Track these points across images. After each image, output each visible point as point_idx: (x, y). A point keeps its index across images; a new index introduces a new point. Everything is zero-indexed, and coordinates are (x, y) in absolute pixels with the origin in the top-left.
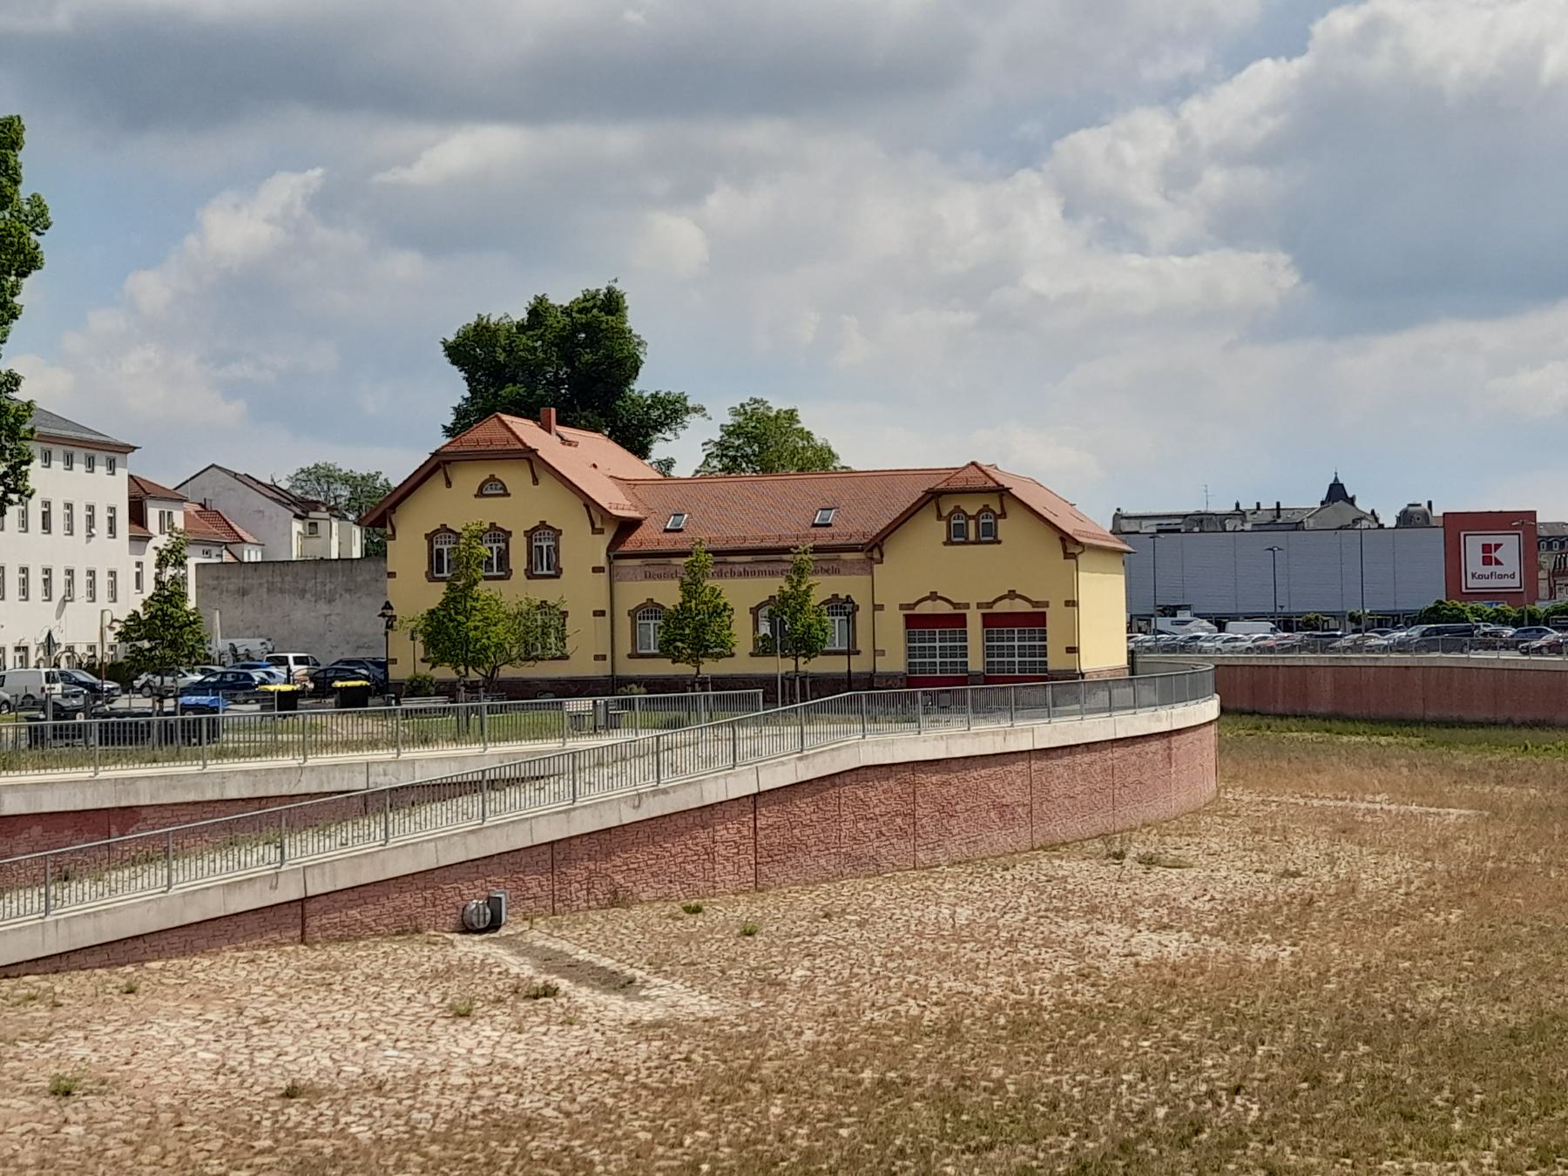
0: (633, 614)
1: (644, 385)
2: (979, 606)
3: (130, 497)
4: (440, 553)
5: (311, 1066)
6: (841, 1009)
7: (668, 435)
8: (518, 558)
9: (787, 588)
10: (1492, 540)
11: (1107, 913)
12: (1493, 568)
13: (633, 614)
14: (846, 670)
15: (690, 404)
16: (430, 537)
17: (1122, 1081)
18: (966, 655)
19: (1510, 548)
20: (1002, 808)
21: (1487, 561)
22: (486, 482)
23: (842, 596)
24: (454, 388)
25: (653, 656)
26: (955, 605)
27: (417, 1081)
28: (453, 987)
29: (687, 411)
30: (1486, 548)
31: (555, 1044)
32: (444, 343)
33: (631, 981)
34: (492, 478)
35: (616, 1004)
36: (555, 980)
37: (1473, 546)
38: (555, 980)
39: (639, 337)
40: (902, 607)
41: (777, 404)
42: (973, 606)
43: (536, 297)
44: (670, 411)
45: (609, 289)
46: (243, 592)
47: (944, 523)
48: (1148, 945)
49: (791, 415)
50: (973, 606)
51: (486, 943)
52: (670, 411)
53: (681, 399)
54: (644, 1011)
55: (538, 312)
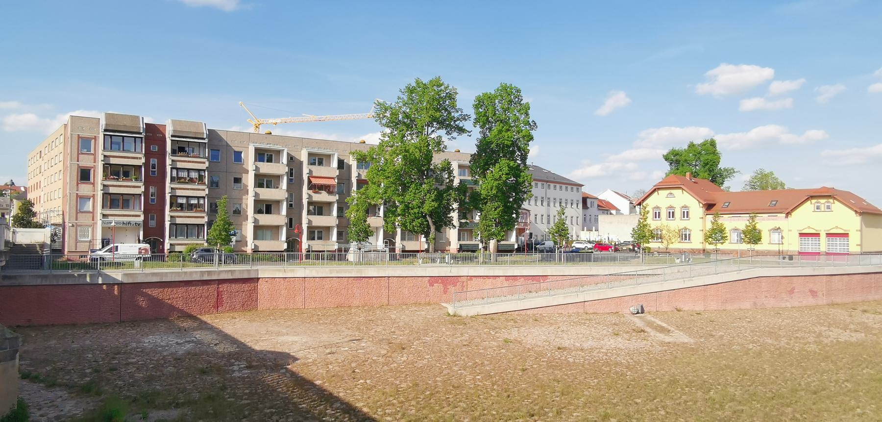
1: (722, 165)
2: (825, 231)
3: (259, 187)
5: (566, 344)
7: (729, 179)
8: (678, 214)
9: (748, 224)
14: (778, 249)
17: (806, 374)
18: (820, 246)
22: (669, 193)
23: (778, 227)
25: (735, 243)
26: (845, 230)
27: (592, 349)
28: (617, 328)
29: (734, 172)
31: (636, 343)
32: (663, 155)
33: (670, 331)
35: (661, 337)
36: (648, 329)
38: (648, 329)
40: (798, 231)
41: (767, 171)
42: (823, 231)
43: (690, 142)
44: (730, 172)
47: (813, 205)
48: (844, 336)
49: (772, 173)
50: (823, 231)
51: (74, 260)
52: (730, 172)
54: (668, 339)
55: (692, 145)
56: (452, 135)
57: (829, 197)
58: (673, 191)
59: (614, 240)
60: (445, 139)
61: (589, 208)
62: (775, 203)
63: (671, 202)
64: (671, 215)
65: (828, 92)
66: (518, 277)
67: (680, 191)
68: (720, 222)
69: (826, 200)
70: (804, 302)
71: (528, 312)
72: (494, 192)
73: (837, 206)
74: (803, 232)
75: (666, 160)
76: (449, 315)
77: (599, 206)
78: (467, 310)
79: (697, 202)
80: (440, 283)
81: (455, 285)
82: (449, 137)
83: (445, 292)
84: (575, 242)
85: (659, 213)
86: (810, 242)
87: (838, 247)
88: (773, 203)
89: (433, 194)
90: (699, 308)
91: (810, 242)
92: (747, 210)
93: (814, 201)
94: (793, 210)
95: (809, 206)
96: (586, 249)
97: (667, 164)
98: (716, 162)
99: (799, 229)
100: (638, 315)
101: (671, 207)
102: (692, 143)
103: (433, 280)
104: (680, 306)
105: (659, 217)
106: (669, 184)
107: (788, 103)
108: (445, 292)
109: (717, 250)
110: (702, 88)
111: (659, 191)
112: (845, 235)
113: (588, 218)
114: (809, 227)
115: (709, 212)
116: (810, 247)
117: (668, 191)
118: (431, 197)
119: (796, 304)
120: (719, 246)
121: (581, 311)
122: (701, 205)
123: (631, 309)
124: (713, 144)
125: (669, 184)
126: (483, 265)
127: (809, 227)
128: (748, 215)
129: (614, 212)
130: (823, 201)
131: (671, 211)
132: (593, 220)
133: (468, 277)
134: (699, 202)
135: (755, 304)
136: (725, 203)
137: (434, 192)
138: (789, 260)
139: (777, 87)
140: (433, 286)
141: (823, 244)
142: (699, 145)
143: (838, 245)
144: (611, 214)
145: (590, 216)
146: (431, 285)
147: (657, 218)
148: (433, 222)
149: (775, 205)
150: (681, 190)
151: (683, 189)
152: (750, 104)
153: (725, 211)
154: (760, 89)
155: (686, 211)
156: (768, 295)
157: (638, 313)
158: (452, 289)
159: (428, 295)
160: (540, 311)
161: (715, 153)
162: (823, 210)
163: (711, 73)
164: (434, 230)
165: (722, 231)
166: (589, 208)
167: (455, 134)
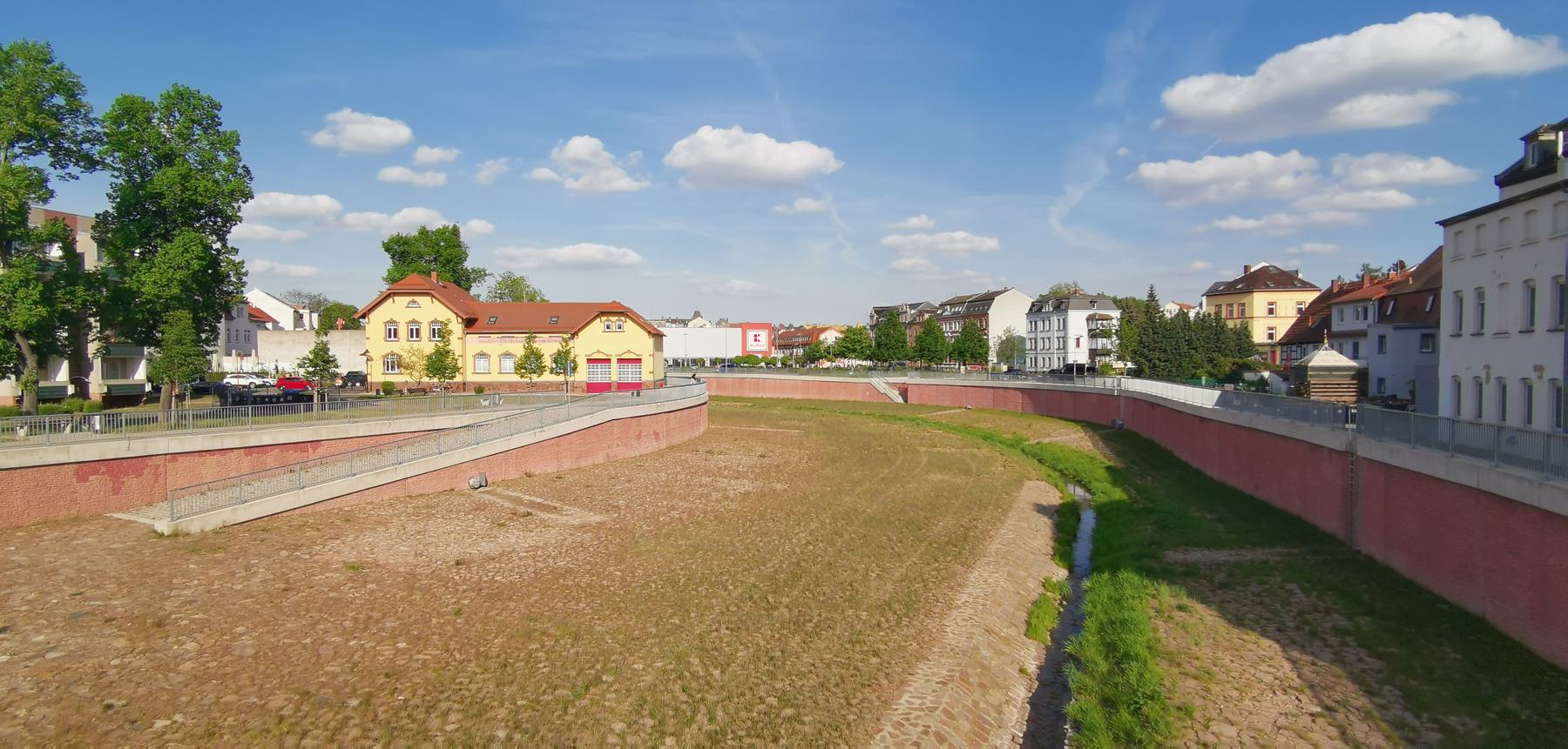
0: (474, 356)
1: (469, 264)
4: (434, 330)
6: (709, 509)
9: (561, 349)
10: (757, 333)
11: (28, 577)
12: (758, 343)
13: (474, 356)
15: (487, 272)
16: (386, 323)
19: (764, 335)
20: (656, 434)
21: (755, 340)
24: (386, 262)
26: (638, 355)
29: (486, 275)
30: (755, 336)
32: (383, 243)
34: (414, 302)
37: (751, 334)
39: (872, 317)
44: (480, 275)
45: (455, 226)
46: (281, 343)
52: (480, 275)
53: (484, 271)
56: (67, 171)
57: (622, 314)
58: (416, 298)
59: (287, 370)
60: (53, 175)
61: (234, 318)
62: (494, 319)
63: (414, 314)
64: (415, 333)
65: (489, 171)
66: (269, 448)
67: (429, 298)
68: (535, 345)
69: (617, 318)
70: (650, 448)
71: (318, 508)
72: (176, 291)
73: (629, 326)
74: (592, 357)
75: (387, 250)
76: (161, 535)
77: (250, 315)
78: (205, 518)
79: (455, 316)
80: (103, 473)
81: (138, 473)
82: (60, 172)
83: (116, 491)
84: (228, 376)
85: (395, 329)
86: (599, 370)
87: (599, 376)
88: (492, 320)
89: (34, 289)
90: (552, 469)
91: (599, 370)
92: (522, 328)
93: (604, 318)
94: (580, 330)
95: (598, 325)
96: (252, 386)
97: (388, 256)
98: (462, 257)
99: (587, 353)
100: (481, 489)
101: (414, 322)
102: (424, 227)
103: (86, 468)
104: (531, 470)
105: (417, 336)
106: (403, 287)
107: (441, 178)
108: (116, 491)
109: (534, 385)
110: (322, 138)
111: (395, 298)
112: (639, 361)
113: (233, 334)
114: (599, 352)
115: (470, 330)
116: (630, 376)
117: (410, 298)
118: (32, 295)
119: (644, 451)
120: (535, 378)
121: (401, 494)
122: (460, 320)
123: (471, 481)
124: (455, 232)
125: (403, 287)
126: (179, 431)
127: (599, 352)
128: (524, 335)
129: (269, 326)
130: (614, 319)
131: (392, 328)
132: (241, 337)
133: (168, 456)
134: (458, 316)
135: (608, 456)
136: (491, 317)
137: (36, 286)
138: (159, 402)
139: (426, 154)
140: (86, 480)
141: (615, 374)
142: (433, 233)
143: (629, 375)
144: (267, 329)
145: (237, 331)
146: (83, 478)
147: (415, 338)
148: (32, 347)
149: (495, 322)
150: (429, 298)
151: (433, 296)
152: (394, 173)
153: (492, 329)
154: (400, 155)
155: (414, 328)
156: (619, 443)
157: (481, 486)
158: (131, 482)
159: (75, 502)
160: (330, 505)
161: (458, 245)
162: (614, 330)
163: (332, 117)
164: (35, 365)
165: (539, 357)
166: (234, 318)
167: (73, 169)
